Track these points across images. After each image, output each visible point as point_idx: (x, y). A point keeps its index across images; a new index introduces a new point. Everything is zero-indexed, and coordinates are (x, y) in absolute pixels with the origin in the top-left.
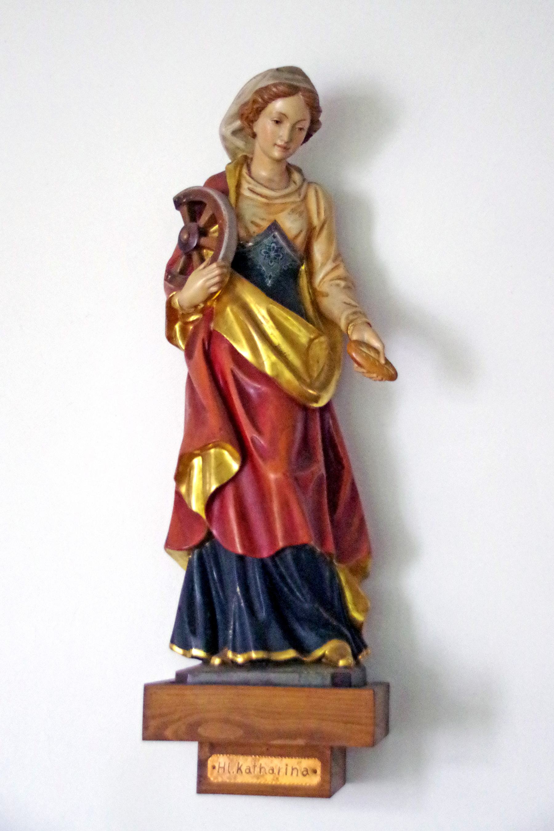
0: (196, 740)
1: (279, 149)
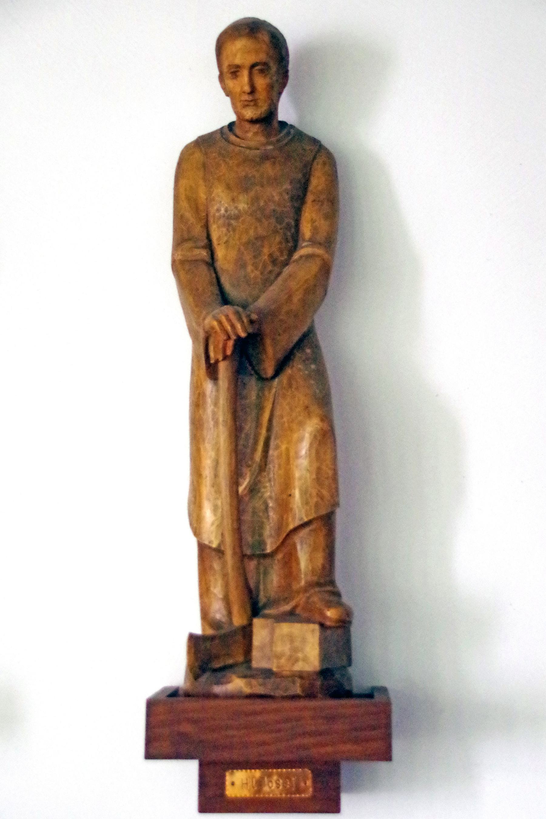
0: (192, 758)
1: (256, 128)
